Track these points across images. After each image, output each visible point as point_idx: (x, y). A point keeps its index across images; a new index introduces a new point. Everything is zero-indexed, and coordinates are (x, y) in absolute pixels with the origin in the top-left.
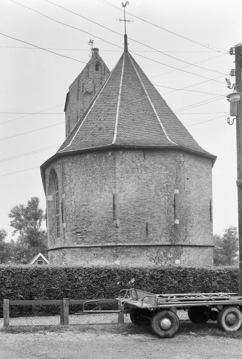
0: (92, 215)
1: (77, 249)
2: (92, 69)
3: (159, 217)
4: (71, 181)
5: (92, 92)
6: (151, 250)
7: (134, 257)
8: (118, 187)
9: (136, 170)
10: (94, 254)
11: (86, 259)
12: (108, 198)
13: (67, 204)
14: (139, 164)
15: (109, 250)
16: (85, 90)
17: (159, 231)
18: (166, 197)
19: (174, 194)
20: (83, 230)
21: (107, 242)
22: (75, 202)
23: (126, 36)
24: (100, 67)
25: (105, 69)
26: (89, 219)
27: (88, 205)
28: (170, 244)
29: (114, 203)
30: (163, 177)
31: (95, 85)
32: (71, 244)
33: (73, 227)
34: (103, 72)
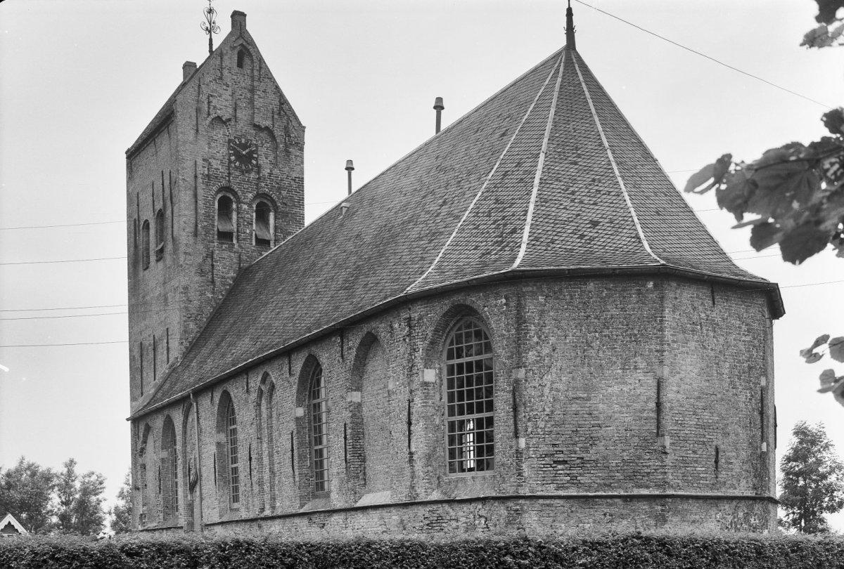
0: (600, 422)
1: (558, 501)
2: (231, 60)
3: (737, 435)
4: (543, 339)
5: (230, 120)
6: (723, 508)
7: (694, 522)
8: (667, 362)
9: (699, 327)
10: (605, 515)
11: (581, 525)
12: (644, 385)
13: (529, 392)
14: (703, 315)
15: (644, 506)
16: (214, 111)
17: (737, 467)
18: (748, 391)
19: (761, 387)
20: (573, 455)
21: (640, 487)
22: (551, 389)
23: (570, 13)
24: (247, 61)
25: (260, 68)
26: (590, 432)
27: (589, 399)
28: (754, 495)
29: (658, 398)
30: (742, 348)
31: (236, 103)
32: (540, 489)
33: (544, 449)
34: (256, 73)
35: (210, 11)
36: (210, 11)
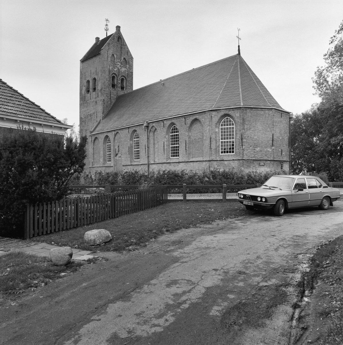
23: (239, 46)
24: (120, 40)
35: (107, 25)
36: (107, 25)
